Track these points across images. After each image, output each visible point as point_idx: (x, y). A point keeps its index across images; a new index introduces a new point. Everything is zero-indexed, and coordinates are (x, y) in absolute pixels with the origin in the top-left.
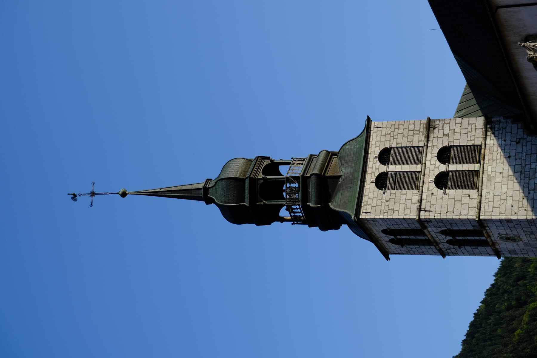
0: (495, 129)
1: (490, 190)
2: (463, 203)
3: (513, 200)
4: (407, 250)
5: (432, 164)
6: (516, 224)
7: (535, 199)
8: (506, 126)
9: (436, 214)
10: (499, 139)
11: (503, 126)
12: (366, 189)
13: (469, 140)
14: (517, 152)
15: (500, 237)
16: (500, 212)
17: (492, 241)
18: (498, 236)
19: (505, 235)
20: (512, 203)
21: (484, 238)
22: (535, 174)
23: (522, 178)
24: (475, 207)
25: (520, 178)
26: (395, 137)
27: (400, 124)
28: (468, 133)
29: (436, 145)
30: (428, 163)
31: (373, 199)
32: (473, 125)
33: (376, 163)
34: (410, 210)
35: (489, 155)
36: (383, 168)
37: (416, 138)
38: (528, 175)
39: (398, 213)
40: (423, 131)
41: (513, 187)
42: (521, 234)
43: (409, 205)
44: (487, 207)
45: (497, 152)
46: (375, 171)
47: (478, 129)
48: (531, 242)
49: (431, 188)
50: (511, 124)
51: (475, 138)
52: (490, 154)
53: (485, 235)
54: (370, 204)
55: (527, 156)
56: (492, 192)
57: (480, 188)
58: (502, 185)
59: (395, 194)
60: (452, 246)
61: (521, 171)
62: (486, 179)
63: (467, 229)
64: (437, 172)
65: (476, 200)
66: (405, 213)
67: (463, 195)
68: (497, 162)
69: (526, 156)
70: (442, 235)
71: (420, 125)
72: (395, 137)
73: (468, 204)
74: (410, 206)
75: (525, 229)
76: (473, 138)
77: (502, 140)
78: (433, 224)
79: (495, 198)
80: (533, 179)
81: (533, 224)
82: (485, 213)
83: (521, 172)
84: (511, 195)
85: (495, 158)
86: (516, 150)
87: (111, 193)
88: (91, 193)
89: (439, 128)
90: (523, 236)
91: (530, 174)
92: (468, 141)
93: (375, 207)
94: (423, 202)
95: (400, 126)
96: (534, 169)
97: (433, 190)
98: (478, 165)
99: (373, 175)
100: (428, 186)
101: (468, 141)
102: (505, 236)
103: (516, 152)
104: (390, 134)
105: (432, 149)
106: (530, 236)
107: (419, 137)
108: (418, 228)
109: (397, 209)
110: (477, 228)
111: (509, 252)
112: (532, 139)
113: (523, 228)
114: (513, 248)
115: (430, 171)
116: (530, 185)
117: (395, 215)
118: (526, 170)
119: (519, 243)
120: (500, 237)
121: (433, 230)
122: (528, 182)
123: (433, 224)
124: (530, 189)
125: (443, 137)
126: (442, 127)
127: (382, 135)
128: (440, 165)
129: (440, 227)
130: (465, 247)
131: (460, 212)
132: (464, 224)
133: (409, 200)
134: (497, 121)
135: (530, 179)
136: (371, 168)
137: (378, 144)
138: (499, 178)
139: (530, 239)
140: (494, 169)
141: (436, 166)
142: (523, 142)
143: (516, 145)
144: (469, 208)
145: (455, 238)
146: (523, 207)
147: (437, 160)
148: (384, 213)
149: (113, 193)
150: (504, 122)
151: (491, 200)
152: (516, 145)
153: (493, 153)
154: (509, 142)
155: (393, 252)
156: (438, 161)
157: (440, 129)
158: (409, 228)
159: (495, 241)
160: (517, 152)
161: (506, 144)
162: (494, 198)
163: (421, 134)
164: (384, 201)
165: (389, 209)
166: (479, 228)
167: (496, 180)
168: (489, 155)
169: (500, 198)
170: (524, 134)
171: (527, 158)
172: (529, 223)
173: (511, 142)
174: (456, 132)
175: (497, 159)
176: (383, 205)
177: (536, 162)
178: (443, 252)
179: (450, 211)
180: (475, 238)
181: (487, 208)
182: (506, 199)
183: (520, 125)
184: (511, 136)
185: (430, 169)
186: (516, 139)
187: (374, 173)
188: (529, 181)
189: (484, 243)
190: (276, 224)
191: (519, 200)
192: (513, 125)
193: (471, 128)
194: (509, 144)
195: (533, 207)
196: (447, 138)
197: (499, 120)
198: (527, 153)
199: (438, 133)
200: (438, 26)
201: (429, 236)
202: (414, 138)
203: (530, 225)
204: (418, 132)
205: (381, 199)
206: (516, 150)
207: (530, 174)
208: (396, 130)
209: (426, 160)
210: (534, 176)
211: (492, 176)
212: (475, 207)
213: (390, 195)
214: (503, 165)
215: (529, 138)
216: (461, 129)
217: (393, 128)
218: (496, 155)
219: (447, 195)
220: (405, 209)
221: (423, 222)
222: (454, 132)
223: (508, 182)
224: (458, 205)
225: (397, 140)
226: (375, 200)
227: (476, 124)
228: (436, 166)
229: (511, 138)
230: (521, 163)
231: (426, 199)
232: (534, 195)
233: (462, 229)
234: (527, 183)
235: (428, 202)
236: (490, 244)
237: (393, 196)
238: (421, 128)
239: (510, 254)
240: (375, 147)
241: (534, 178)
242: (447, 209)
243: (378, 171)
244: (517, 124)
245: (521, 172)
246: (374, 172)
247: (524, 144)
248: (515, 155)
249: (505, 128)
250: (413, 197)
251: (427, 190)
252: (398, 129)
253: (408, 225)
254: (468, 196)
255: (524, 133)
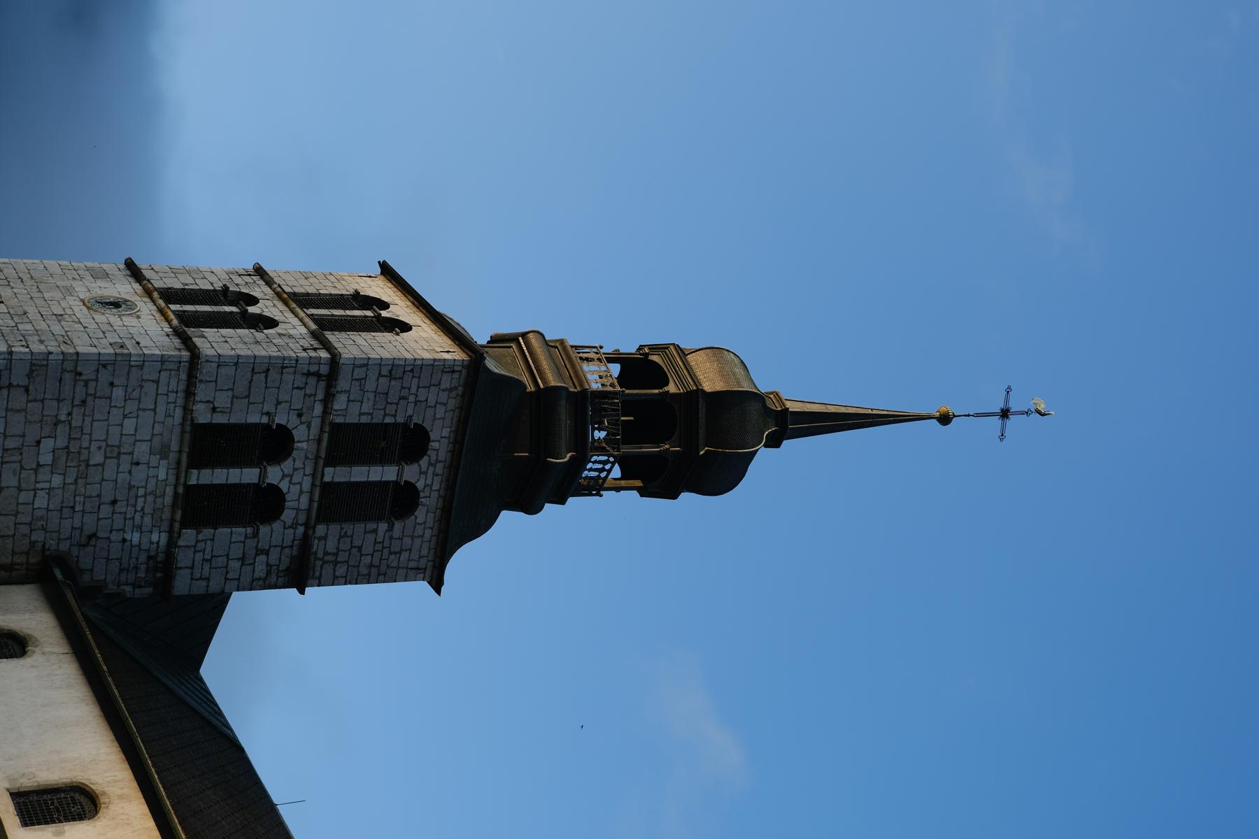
0: (147, 568)
1: (163, 423)
2: (230, 393)
3: (110, 398)
4: (343, 282)
5: (299, 483)
6: (100, 340)
7: (56, 399)
8: (119, 574)
9: (293, 367)
10: (138, 543)
11: (127, 575)
12: (451, 427)
13: (209, 542)
14: (96, 514)
15: (134, 309)
16: (142, 369)
17: (153, 301)
18: (139, 311)
19: (125, 315)
20: (112, 392)
21: (173, 307)
22: (53, 461)
23: (86, 452)
24: (201, 381)
25: (89, 452)
26: (379, 547)
27: (368, 577)
28: (209, 557)
29: (286, 529)
30: (307, 486)
31: (437, 403)
32: (198, 576)
33: (426, 486)
34: (352, 376)
35: (162, 507)
36: (410, 473)
37: (331, 545)
38: (70, 457)
39: (380, 370)
40: (315, 561)
41: (108, 430)
42: (86, 315)
43: (355, 387)
44: (173, 382)
45: (144, 513)
46: (428, 468)
47: (186, 567)
48: (58, 295)
49: (303, 427)
50: (108, 581)
51: (195, 547)
52: (160, 509)
53: (172, 316)
54: (443, 390)
55: (72, 504)
56: (160, 417)
57: (188, 428)
58: (134, 435)
59: (385, 415)
60: (245, 290)
61: (87, 469)
62: (172, 449)
63: (216, 330)
64: (287, 465)
65: (197, 398)
66: (365, 369)
67: (228, 410)
68: (144, 489)
69: (74, 504)
70: (272, 316)
71: (321, 574)
72: (379, 547)
73: (218, 388)
74: (352, 387)
75: (78, 326)
76: (200, 546)
77: (131, 541)
78: (298, 342)
79: (153, 402)
80: (58, 449)
81: (61, 339)
82: (179, 367)
83: (88, 465)
84: (114, 411)
85: (150, 499)
86: (99, 519)
87: (969, 415)
88: (1007, 417)
89: (278, 569)
90: (82, 313)
91: (66, 462)
92: (212, 538)
93: (432, 384)
94: (320, 396)
95: (366, 571)
96: (56, 473)
97: (299, 422)
98: (189, 481)
99: (433, 458)
100: (309, 432)
101: (212, 540)
102: (123, 313)
103: (98, 512)
104: (391, 553)
105: (297, 520)
106: (64, 309)
107: (325, 548)
108: (329, 333)
109: (382, 380)
110: (193, 332)
111: (107, 274)
112: (58, 544)
113: (83, 329)
114: (100, 283)
115: (304, 469)
116: (67, 436)
117: (388, 365)
118: (76, 469)
119: (88, 294)
120: (135, 311)
121: (295, 328)
122: (72, 442)
123: (298, 342)
124: (68, 425)
125: (270, 546)
126: (270, 570)
127: (408, 552)
128: (280, 482)
129: (280, 335)
130: (213, 288)
131: (236, 370)
132: (226, 342)
133: (354, 401)
134: (140, 587)
135: (67, 447)
136: (437, 475)
137: (419, 530)
138: (142, 450)
139: (62, 302)
140: (152, 472)
141: (287, 479)
142: (81, 536)
143: (97, 530)
144: (215, 379)
145: (240, 309)
146: (86, 383)
147: (287, 493)
148: (412, 371)
149: (965, 416)
150: (123, 585)
151: (161, 399)
152: (97, 530)
153: (154, 510)
154: (115, 536)
155: (373, 281)
156: (285, 490)
157: (276, 567)
158: (351, 333)
159: (145, 299)
160: (96, 514)
161: (122, 532)
162: (156, 403)
163: (320, 555)
164: (412, 398)
165: (402, 378)
166: (191, 331)
167: (149, 447)
168: (162, 507)
169: (140, 402)
170: (77, 557)
171: (72, 498)
172: (69, 342)
173: (108, 538)
174: (238, 559)
175: (145, 496)
176: (413, 390)
177: (51, 491)
178: (262, 278)
179: (260, 373)
180: (194, 309)
181: (172, 381)
182: (125, 401)
183: (87, 577)
184: (109, 551)
185: (302, 473)
186: (98, 544)
187: (430, 464)
188: (69, 443)
189: (170, 296)
190: (629, 348)
191: (95, 398)
192: (103, 577)
193: (202, 569)
194: (114, 532)
195: (61, 379)
196: (260, 544)
197: (136, 590)
198: (72, 511)
199: (280, 558)
200: (282, 810)
201: (302, 314)
202: (336, 544)
203: (66, 337)
204: (327, 558)
205: (418, 403)
206: (34, 509)
207: (66, 462)
208: (376, 562)
209: (311, 492)
210: (56, 456)
211: (158, 456)
212: (201, 381)
213: (396, 411)
214: (130, 482)
215: (64, 547)
216: (226, 567)
217: (383, 568)
218: (146, 506)
219: (265, 410)
220: (365, 379)
221: (322, 347)
222: (242, 559)
223: (120, 442)
224: (241, 388)
225: (376, 540)
226: (432, 401)
227: (192, 579)
228: (287, 479)
229: (109, 546)
230: (88, 486)
231: (315, 401)
232: (58, 411)
233: (228, 330)
234: (74, 439)
235: (310, 396)
236: (156, 295)
237: (391, 409)
238: (319, 569)
239: (105, 271)
240: (425, 523)
241: (56, 452)
242: (266, 377)
243: (420, 469)
244: (92, 580)
245: (88, 465)
246: (432, 465)
247: (78, 532)
248: (101, 507)
249: (121, 571)
250: (345, 408)
251: (313, 424)
252: (371, 566)
253: (354, 342)
254: (218, 410)
255: (76, 559)
